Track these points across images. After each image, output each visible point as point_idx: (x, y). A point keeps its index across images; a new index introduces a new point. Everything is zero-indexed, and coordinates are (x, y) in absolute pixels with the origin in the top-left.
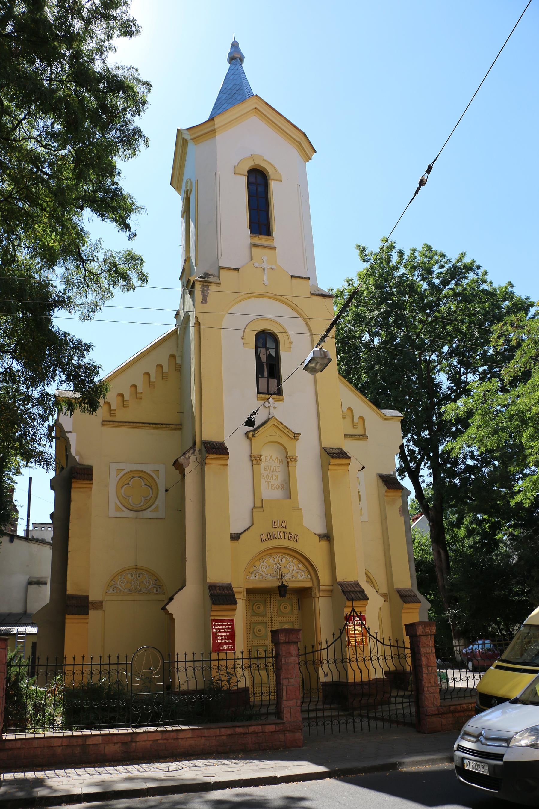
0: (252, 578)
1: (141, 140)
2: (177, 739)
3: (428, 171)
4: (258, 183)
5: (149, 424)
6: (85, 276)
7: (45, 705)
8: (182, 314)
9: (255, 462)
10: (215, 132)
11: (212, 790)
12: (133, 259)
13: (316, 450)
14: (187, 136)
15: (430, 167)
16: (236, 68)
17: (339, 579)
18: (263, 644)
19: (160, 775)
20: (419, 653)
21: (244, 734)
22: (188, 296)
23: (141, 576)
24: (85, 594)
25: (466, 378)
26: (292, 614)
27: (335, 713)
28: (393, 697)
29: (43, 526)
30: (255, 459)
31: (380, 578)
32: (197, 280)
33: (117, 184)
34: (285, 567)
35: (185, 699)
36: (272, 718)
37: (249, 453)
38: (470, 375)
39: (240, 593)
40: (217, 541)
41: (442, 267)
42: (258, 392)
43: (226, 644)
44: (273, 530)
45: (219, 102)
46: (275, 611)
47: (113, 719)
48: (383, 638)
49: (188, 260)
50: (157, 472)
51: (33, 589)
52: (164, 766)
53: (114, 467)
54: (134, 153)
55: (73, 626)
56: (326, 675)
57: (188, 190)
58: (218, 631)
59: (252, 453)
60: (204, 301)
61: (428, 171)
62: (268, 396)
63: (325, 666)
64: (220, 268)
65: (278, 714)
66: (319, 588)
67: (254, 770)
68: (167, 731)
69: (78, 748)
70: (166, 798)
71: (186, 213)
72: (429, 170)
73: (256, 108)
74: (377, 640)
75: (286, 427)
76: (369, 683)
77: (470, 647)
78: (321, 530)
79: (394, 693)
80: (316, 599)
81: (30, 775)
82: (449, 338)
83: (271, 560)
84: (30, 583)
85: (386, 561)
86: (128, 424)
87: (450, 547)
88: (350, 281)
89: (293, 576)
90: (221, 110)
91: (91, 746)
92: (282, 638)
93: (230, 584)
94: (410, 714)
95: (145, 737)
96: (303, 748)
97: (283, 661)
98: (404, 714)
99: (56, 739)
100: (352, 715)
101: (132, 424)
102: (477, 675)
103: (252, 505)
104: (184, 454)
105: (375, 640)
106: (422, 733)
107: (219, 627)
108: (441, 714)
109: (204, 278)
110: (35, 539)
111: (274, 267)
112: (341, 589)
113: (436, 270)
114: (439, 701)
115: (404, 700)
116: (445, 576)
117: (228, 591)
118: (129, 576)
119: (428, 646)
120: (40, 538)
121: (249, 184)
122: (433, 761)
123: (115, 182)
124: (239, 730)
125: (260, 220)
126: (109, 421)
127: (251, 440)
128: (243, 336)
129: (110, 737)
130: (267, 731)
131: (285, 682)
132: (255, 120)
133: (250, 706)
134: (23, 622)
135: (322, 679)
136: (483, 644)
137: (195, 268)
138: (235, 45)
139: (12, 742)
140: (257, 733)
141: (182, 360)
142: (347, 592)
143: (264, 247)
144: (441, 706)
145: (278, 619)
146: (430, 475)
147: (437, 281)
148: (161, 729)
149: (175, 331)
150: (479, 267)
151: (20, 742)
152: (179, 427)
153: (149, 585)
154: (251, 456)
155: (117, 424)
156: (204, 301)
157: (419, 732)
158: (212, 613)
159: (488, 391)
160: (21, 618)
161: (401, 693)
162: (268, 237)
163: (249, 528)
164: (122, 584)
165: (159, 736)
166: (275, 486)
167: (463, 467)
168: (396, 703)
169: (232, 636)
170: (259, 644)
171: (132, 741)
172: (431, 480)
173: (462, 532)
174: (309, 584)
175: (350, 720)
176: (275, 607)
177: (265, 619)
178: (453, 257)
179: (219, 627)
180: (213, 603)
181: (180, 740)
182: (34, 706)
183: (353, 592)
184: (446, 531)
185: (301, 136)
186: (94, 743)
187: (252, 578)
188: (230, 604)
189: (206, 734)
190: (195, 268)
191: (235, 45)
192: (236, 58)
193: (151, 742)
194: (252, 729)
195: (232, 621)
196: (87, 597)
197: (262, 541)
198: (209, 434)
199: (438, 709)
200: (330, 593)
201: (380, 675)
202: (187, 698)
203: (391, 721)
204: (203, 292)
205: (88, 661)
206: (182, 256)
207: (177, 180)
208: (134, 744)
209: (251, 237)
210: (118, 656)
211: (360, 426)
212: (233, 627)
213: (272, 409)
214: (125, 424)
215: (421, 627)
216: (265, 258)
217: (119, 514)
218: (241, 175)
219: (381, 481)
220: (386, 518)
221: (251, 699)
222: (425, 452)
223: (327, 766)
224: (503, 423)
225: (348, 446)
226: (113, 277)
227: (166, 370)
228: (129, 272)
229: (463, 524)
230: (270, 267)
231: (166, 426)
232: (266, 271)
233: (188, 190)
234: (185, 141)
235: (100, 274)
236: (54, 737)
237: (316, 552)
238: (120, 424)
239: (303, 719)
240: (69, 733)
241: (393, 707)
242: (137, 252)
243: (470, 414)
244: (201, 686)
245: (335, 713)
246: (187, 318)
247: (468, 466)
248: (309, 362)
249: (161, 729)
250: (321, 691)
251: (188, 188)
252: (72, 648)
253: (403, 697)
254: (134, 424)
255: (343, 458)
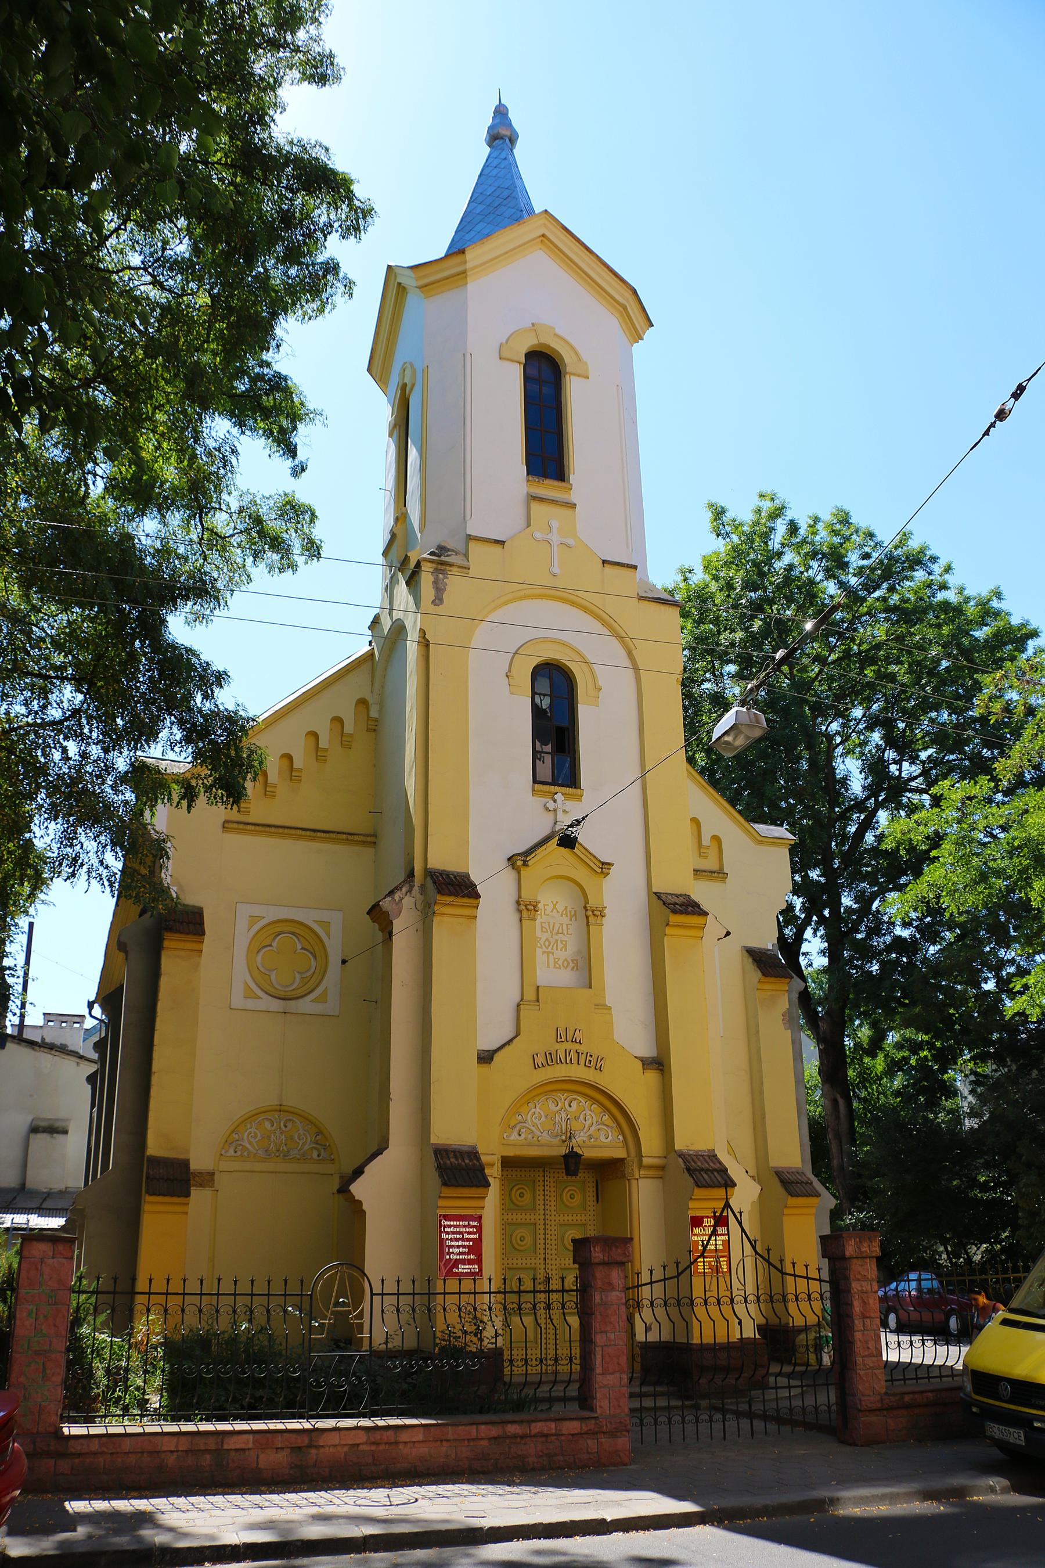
0: (514, 1136)
1: (339, 285)
2: (397, 1443)
3: (1016, 396)
4: (545, 377)
5: (314, 831)
6: (202, 538)
7: (127, 1370)
8: (386, 624)
9: (525, 914)
10: (466, 277)
11: (486, 1543)
12: (294, 511)
13: (641, 897)
14: (408, 280)
15: (1021, 389)
16: (503, 156)
17: (679, 1145)
18: (529, 1265)
19: (380, 1513)
20: (848, 1291)
21: (522, 1437)
22: (402, 588)
23: (289, 1125)
24: (182, 1157)
25: (900, 770)
26: (585, 1209)
27: (662, 1402)
28: (772, 1375)
29: (64, 1019)
30: (525, 908)
31: (745, 1145)
32: (425, 560)
33: (268, 365)
34: (576, 1118)
35: (396, 1367)
36: (574, 1407)
37: (515, 897)
38: (905, 765)
39: (492, 1165)
40: (451, 1061)
41: (866, 556)
42: (535, 781)
43: (463, 1262)
44: (558, 1046)
45: (468, 219)
46: (553, 1203)
47: (271, 1403)
48: (768, 1250)
49: (401, 517)
50: (326, 924)
51: (39, 1141)
52: (379, 1494)
53: (245, 911)
54: (321, 310)
55: (157, 1217)
56: (648, 1329)
57: (405, 385)
58: (450, 1236)
59: (520, 897)
60: (438, 600)
61: (1016, 396)
62: (553, 788)
63: (647, 1313)
64: (470, 538)
65: (585, 1400)
66: (640, 1161)
67: (556, 1506)
68: (377, 1428)
69: (208, 1457)
70: (402, 1555)
71: (402, 427)
72: (1019, 391)
73: (543, 235)
74: (770, 1264)
75: (586, 849)
76: (728, 1347)
77: (894, 1285)
78: (645, 1048)
79: (775, 1368)
80: (634, 1182)
81: (122, 1505)
82: (863, 692)
83: (550, 1103)
84: (35, 1130)
85: (754, 1114)
86: (273, 830)
87: (854, 1092)
88: (686, 573)
89: (590, 1137)
90: (472, 233)
91: (233, 1453)
92: (597, 1254)
93: (474, 1147)
94: (816, 1408)
95: (335, 1439)
96: (632, 1467)
97: (597, 1298)
98: (803, 1409)
99: (166, 1438)
100: (696, 1407)
101: (281, 830)
102: (905, 1339)
103: (517, 998)
104: (391, 893)
105: (766, 1265)
106: (851, 1445)
107: (452, 1229)
108: (886, 1409)
109: (439, 556)
110: (47, 1044)
111: (570, 541)
112: (683, 1165)
113: (854, 559)
114: (883, 1383)
115: (793, 1383)
116: (846, 1147)
117: (471, 1160)
118: (267, 1125)
119: (865, 1278)
120: (58, 1042)
121: (527, 379)
122: (892, 1498)
123: (266, 361)
124: (512, 1429)
125: (546, 452)
126: (238, 823)
127: (519, 873)
128: (510, 671)
129: (268, 1435)
130: (565, 1432)
131: (599, 1339)
132: (539, 258)
133: (505, 1383)
134: (19, 1206)
135: (640, 1337)
136: (919, 1280)
137: (419, 535)
138: (501, 112)
139: (81, 1441)
140: (546, 1436)
141: (380, 711)
142: (696, 1170)
143: (553, 502)
144: (886, 1393)
145: (557, 1218)
146: (823, 952)
147: (853, 581)
148: (365, 1422)
149: (370, 655)
150: (934, 559)
151: (96, 1441)
152: (372, 839)
153: (304, 1144)
154: (518, 903)
155: (253, 828)
156: (438, 600)
157: (842, 1442)
158: (441, 1203)
159: (969, 798)
160: (15, 1198)
161: (787, 1369)
162: (561, 484)
163: (511, 1040)
164: (252, 1140)
165: (362, 1437)
166: (560, 962)
167: (888, 939)
168: (776, 1388)
169: (476, 1248)
170: (519, 1266)
171: (310, 1446)
172: (825, 961)
173: (879, 1064)
174: (620, 1154)
175: (690, 1418)
176: (552, 1194)
177: (533, 1217)
178: (887, 536)
179: (452, 1229)
180: (445, 1184)
181: (401, 1446)
182: (108, 1371)
183: (706, 1171)
184: (849, 1060)
185: (628, 294)
186: (238, 1447)
187: (514, 1136)
188: (477, 1186)
189: (450, 1436)
190: (419, 535)
191: (501, 112)
192: (501, 136)
193: (346, 1449)
194: (538, 1427)
195: (479, 1219)
196: (185, 1164)
197: (536, 1067)
198: (441, 858)
199: (882, 1400)
200: (660, 1171)
201: (750, 1332)
202: (401, 1364)
203: (779, 1420)
204: (435, 583)
205: (227, 1287)
206: (386, 510)
207: (380, 364)
208: (313, 1451)
209: (528, 481)
210: (286, 1281)
211: (713, 854)
212: (479, 1229)
213: (560, 813)
214: (267, 829)
215: (852, 1242)
216: (555, 524)
217: (251, 1004)
218: (512, 361)
219: (750, 960)
220: (758, 1032)
221: (507, 1371)
222: (812, 908)
223: (696, 1502)
224: (995, 860)
225: (701, 892)
226: (254, 544)
227: (349, 728)
228: (285, 536)
229: (881, 1049)
230: (564, 540)
231: (346, 837)
232: (555, 548)
233: (405, 385)
234: (401, 289)
235: (232, 536)
236: (163, 1434)
237: (636, 1092)
238: (258, 828)
239: (632, 1410)
240: (172, 1428)
241: (771, 1394)
242: (303, 497)
243: (936, 840)
244: (410, 1343)
245: (662, 1402)
246: (399, 630)
247: (898, 939)
248: (726, 733)
249: (365, 1422)
250: (639, 1359)
251: (406, 381)
252: (154, 1262)
253: (789, 1376)
254: (286, 831)
255: (693, 913)
